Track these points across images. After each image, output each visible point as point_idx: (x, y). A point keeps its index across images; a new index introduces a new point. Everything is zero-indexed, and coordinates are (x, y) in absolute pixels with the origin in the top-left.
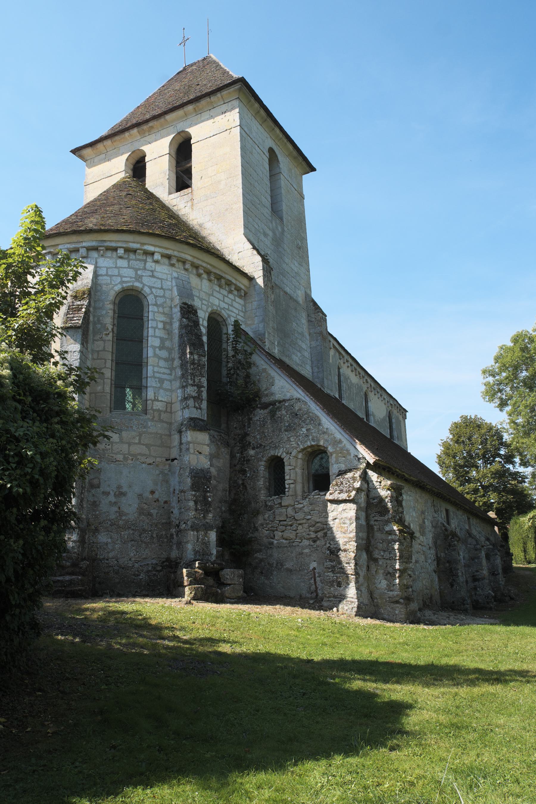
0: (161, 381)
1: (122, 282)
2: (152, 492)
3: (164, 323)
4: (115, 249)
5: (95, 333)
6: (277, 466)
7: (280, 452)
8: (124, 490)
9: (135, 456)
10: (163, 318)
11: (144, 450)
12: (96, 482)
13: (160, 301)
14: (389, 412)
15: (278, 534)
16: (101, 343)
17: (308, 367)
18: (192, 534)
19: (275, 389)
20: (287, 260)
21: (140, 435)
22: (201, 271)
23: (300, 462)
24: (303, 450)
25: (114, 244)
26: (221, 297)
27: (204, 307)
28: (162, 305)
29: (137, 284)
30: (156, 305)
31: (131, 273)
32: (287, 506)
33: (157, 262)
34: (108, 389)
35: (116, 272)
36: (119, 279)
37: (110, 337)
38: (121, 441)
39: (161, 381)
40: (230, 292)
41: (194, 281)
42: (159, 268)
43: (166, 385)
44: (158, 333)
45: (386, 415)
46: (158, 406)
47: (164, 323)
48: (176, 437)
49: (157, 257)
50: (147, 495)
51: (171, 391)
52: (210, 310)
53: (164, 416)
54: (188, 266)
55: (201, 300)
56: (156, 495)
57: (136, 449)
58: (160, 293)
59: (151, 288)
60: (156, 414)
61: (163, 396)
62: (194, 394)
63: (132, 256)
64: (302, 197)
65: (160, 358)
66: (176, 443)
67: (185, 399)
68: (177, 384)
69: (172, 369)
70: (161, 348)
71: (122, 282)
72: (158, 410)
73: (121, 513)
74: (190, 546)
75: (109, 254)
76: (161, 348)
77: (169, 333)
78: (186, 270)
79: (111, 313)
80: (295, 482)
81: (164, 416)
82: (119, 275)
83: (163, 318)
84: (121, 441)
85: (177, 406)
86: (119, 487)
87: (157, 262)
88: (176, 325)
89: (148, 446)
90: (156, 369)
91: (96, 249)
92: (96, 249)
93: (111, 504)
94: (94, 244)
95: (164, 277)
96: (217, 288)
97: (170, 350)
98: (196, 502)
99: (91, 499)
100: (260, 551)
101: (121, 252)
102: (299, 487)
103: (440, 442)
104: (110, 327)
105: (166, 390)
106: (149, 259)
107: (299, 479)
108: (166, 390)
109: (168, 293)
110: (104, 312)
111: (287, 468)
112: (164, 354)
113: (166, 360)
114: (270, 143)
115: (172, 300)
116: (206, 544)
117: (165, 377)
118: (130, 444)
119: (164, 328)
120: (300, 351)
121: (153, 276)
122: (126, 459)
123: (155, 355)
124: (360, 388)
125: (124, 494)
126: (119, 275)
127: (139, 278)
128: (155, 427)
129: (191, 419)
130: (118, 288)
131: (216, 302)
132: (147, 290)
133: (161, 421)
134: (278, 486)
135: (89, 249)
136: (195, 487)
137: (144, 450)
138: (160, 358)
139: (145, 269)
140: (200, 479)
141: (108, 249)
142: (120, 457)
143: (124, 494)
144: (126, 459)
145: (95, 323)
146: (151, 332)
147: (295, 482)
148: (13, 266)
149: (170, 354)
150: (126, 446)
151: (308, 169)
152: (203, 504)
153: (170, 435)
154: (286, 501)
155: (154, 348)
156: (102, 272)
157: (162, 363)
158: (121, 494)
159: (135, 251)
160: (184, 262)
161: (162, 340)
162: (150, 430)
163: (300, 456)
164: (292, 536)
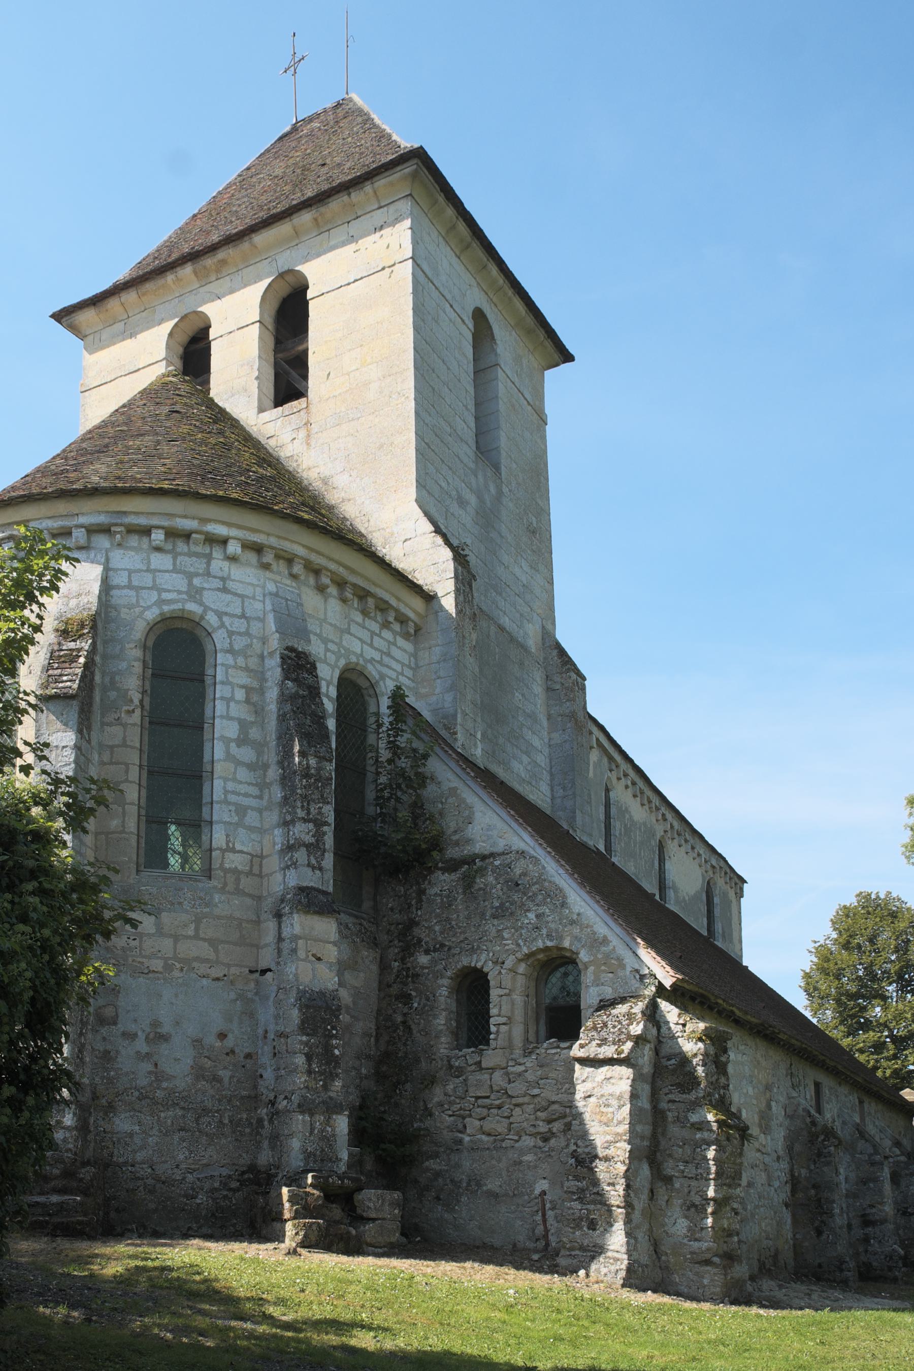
0: (241, 811)
1: (161, 602)
2: (222, 1036)
3: (248, 690)
4: (146, 531)
6: (474, 986)
7: (481, 961)
8: (165, 1029)
9: (187, 963)
10: (243, 679)
11: (205, 950)
12: (109, 1012)
13: (239, 643)
16: (117, 730)
17: (545, 788)
18: (299, 1121)
19: (475, 830)
21: (198, 921)
22: (325, 580)
23: (521, 981)
25: (143, 521)
26: (366, 635)
28: (243, 653)
30: (230, 651)
31: (180, 582)
33: (233, 559)
34: (132, 825)
35: (148, 580)
36: (154, 596)
37: (136, 717)
38: (160, 932)
39: (241, 811)
41: (311, 600)
43: (252, 818)
44: (236, 710)
46: (234, 861)
47: (248, 690)
48: (271, 925)
49: (233, 548)
50: (211, 1039)
51: (261, 831)
52: (342, 663)
54: (297, 569)
55: (325, 641)
56: (230, 1042)
57: (189, 949)
58: (239, 625)
59: (220, 615)
60: (231, 878)
61: (244, 842)
62: (309, 839)
63: (181, 546)
64: (543, 420)
65: (238, 763)
66: (270, 938)
67: (289, 848)
68: (274, 817)
69: (263, 786)
70: (242, 741)
71: (161, 602)
72: (235, 871)
73: (159, 1076)
74: (296, 1144)
75: (134, 540)
76: (242, 741)
77: (259, 711)
78: (294, 577)
79: (138, 667)
81: (245, 882)
82: (154, 587)
84: (160, 932)
85: (273, 863)
86: (156, 1024)
87: (233, 559)
90: (230, 786)
91: (105, 530)
92: (105, 530)
94: (102, 519)
95: (249, 591)
96: (359, 618)
98: (309, 1057)
101: (158, 536)
102: (518, 1032)
104: (136, 697)
105: (251, 829)
106: (217, 553)
108: (251, 829)
110: (124, 665)
111: (494, 993)
112: (247, 754)
113: (251, 767)
115: (264, 640)
116: (328, 1140)
117: (246, 801)
118: (176, 938)
119: (247, 701)
120: (527, 753)
121: (225, 590)
123: (229, 757)
125: (164, 1038)
126: (154, 587)
127: (195, 594)
128: (227, 906)
129: (301, 889)
130: (152, 615)
131: (356, 647)
132: (212, 619)
133: (238, 892)
135: (92, 530)
137: (205, 950)
138: (238, 763)
139: (208, 574)
140: (318, 1011)
141: (131, 530)
142: (157, 965)
143: (164, 1038)
144: (168, 968)
145: (104, 689)
146: (220, 707)
147: (510, 1021)
149: (259, 754)
152: (324, 1061)
153: (258, 922)
155: (226, 741)
157: (243, 774)
159: (187, 536)
162: (217, 911)
163: (522, 968)
164: (501, 1128)
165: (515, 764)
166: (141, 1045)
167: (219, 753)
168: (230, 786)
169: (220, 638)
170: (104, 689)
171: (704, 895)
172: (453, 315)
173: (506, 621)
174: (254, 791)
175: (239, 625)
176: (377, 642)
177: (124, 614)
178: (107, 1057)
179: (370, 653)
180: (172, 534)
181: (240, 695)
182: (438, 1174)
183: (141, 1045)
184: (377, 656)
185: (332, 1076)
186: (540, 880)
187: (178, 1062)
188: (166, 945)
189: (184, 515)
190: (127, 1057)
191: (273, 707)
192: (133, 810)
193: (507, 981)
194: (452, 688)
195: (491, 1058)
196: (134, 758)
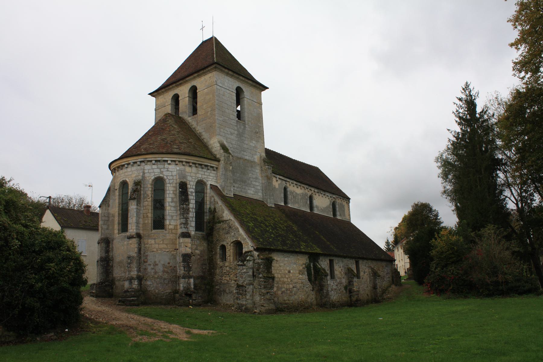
0: (172, 216)
1: (155, 175)
2: (169, 263)
3: (173, 191)
4: (151, 161)
5: (144, 199)
6: (223, 248)
7: (225, 243)
8: (157, 263)
9: (161, 249)
10: (173, 189)
11: (165, 246)
12: (146, 260)
13: (171, 181)
14: (333, 203)
15: (224, 278)
16: (147, 203)
17: (260, 194)
18: (182, 280)
19: (224, 215)
20: (246, 142)
21: (163, 240)
22: (191, 164)
23: (232, 247)
24: (232, 242)
25: (150, 159)
26: (203, 173)
27: (193, 180)
28: (172, 183)
29: (161, 175)
30: (169, 183)
31: (158, 170)
32: (227, 267)
33: (169, 164)
34: (150, 222)
35: (152, 171)
36: (153, 174)
37: (150, 199)
38: (155, 243)
39: (172, 216)
40: (208, 169)
41: (188, 169)
42: (170, 166)
43: (174, 218)
44: (170, 196)
45: (330, 204)
46: (171, 227)
47: (173, 191)
48: (178, 240)
49: (169, 162)
50: (166, 264)
51: (177, 220)
52: (196, 180)
53: (173, 231)
54: (184, 163)
55: (192, 177)
56: (171, 265)
57: (162, 246)
58: (171, 178)
59: (167, 176)
60: (170, 231)
61: (173, 223)
62: (184, 222)
63: (159, 163)
64: (261, 104)
65: (171, 206)
66: (178, 243)
67: (181, 224)
68: (178, 218)
69: (176, 211)
70: (172, 202)
71: (155, 175)
72: (171, 229)
73: (156, 273)
74: (181, 285)
75: (149, 163)
76: (172, 202)
77: (175, 195)
78: (184, 165)
79: (150, 189)
80: (230, 256)
81: (173, 231)
82: (153, 172)
83: (173, 189)
84: (155, 243)
85: (179, 227)
86: (155, 262)
87: (169, 164)
88: (178, 191)
89: (166, 244)
90: (170, 211)
91: (143, 162)
92: (143, 162)
93: (152, 269)
94: (142, 160)
95: (173, 170)
96: (201, 169)
97: (176, 202)
98: (184, 267)
99: (144, 267)
100: (217, 285)
101: (154, 162)
102: (232, 258)
103: (412, 204)
104: (150, 195)
105: (175, 220)
106: (166, 163)
107: (232, 255)
108: (175, 220)
109: (175, 178)
110: (147, 189)
111: (227, 250)
112: (173, 204)
113: (174, 207)
114: (237, 84)
115: (176, 180)
116: (189, 284)
117: (173, 214)
118: (159, 244)
119: (173, 193)
120: (254, 187)
121: (168, 171)
122: (157, 250)
123: (169, 206)
124: (306, 195)
125: (157, 265)
126: (153, 172)
127: (162, 172)
128: (170, 236)
129: (182, 233)
130: (153, 178)
131: (200, 176)
132: (165, 177)
133: (172, 233)
134: (224, 258)
135: (141, 162)
136: (184, 261)
137: (165, 246)
138: (171, 206)
139: (164, 168)
140: (186, 257)
141: (148, 161)
142: (155, 250)
143: (157, 265)
144: (157, 250)
145: (144, 194)
146: (167, 196)
147: (230, 256)
148: (30, 268)
149: (176, 204)
150: (157, 245)
151: (262, 88)
152: (188, 268)
153: (176, 239)
154: (227, 264)
155: (169, 202)
156: (146, 171)
157: (172, 209)
158: (156, 264)
159: (159, 161)
160: (182, 162)
161: (172, 198)
162: (167, 238)
163: (232, 245)
164: (228, 279)
165: (249, 191)
166: (152, 266)
167: (167, 205)
168: (170, 211)
169: (167, 181)
170: (144, 194)
171: (331, 206)
172: (228, 92)
173: (247, 158)
174: (175, 212)
175: (171, 178)
176: (206, 173)
177: (147, 178)
178: (145, 269)
179: (204, 176)
180: (156, 161)
181: (171, 192)
182: (218, 289)
183: (152, 266)
184: (206, 177)
185: (190, 271)
186: (234, 226)
187: (160, 268)
188: (157, 246)
189: (159, 157)
190: (149, 269)
191: (178, 194)
192: (150, 219)
193: (229, 247)
194: (224, 181)
195: (227, 264)
196: (150, 208)
